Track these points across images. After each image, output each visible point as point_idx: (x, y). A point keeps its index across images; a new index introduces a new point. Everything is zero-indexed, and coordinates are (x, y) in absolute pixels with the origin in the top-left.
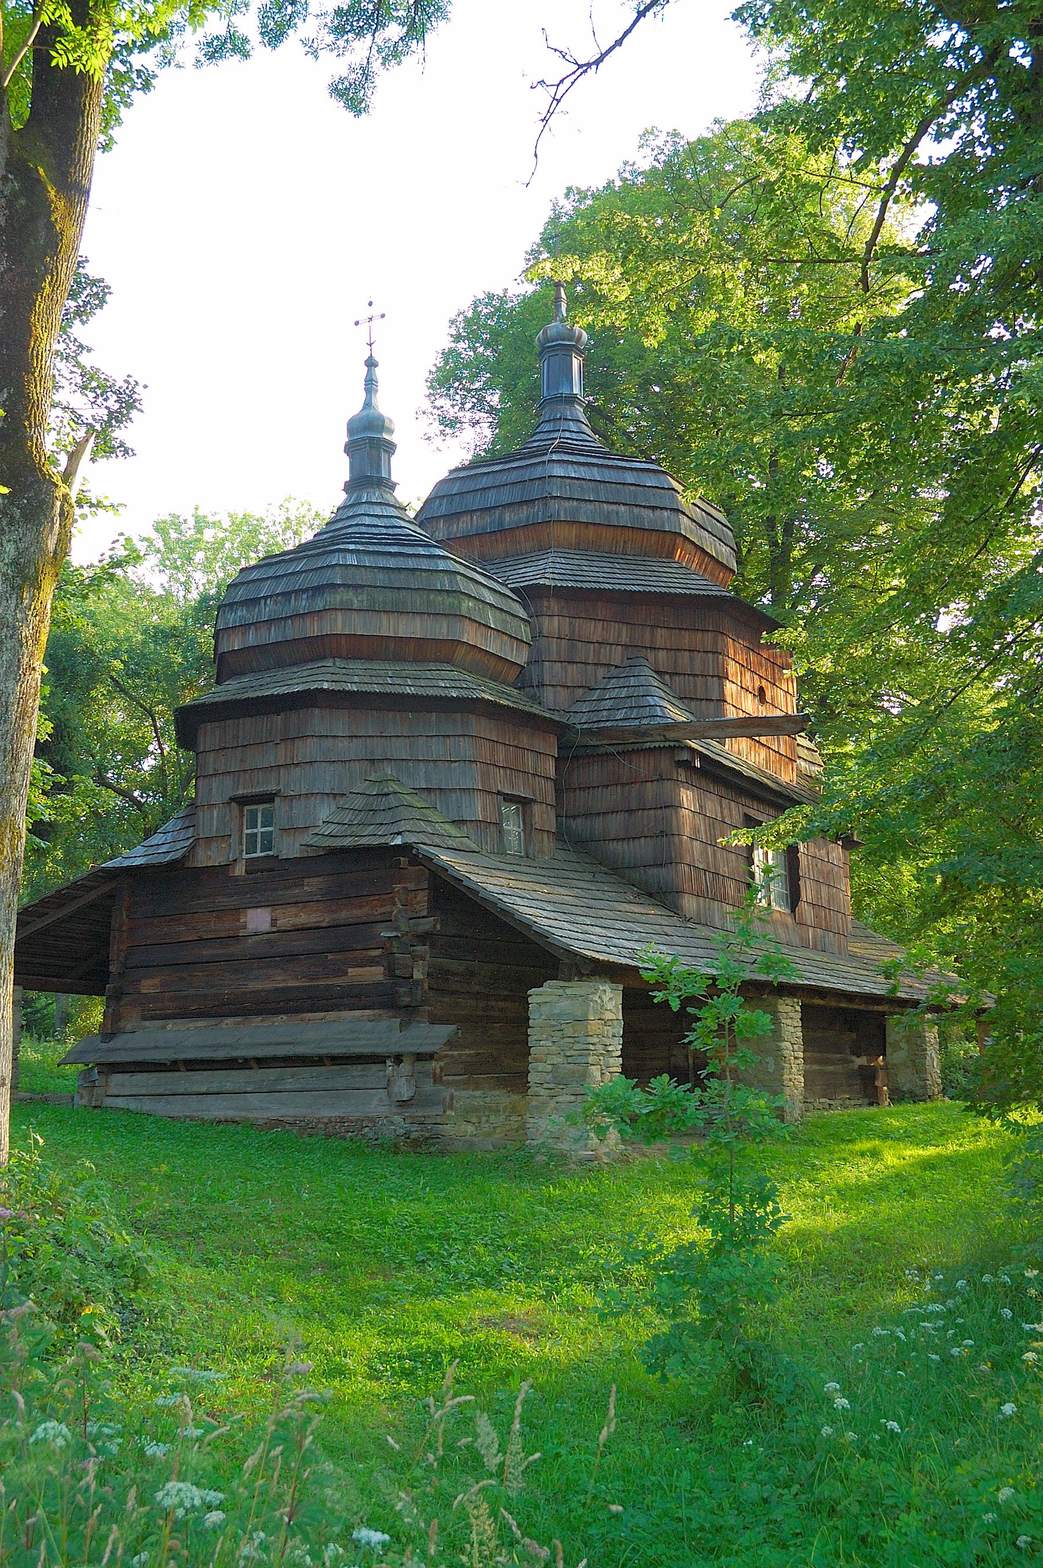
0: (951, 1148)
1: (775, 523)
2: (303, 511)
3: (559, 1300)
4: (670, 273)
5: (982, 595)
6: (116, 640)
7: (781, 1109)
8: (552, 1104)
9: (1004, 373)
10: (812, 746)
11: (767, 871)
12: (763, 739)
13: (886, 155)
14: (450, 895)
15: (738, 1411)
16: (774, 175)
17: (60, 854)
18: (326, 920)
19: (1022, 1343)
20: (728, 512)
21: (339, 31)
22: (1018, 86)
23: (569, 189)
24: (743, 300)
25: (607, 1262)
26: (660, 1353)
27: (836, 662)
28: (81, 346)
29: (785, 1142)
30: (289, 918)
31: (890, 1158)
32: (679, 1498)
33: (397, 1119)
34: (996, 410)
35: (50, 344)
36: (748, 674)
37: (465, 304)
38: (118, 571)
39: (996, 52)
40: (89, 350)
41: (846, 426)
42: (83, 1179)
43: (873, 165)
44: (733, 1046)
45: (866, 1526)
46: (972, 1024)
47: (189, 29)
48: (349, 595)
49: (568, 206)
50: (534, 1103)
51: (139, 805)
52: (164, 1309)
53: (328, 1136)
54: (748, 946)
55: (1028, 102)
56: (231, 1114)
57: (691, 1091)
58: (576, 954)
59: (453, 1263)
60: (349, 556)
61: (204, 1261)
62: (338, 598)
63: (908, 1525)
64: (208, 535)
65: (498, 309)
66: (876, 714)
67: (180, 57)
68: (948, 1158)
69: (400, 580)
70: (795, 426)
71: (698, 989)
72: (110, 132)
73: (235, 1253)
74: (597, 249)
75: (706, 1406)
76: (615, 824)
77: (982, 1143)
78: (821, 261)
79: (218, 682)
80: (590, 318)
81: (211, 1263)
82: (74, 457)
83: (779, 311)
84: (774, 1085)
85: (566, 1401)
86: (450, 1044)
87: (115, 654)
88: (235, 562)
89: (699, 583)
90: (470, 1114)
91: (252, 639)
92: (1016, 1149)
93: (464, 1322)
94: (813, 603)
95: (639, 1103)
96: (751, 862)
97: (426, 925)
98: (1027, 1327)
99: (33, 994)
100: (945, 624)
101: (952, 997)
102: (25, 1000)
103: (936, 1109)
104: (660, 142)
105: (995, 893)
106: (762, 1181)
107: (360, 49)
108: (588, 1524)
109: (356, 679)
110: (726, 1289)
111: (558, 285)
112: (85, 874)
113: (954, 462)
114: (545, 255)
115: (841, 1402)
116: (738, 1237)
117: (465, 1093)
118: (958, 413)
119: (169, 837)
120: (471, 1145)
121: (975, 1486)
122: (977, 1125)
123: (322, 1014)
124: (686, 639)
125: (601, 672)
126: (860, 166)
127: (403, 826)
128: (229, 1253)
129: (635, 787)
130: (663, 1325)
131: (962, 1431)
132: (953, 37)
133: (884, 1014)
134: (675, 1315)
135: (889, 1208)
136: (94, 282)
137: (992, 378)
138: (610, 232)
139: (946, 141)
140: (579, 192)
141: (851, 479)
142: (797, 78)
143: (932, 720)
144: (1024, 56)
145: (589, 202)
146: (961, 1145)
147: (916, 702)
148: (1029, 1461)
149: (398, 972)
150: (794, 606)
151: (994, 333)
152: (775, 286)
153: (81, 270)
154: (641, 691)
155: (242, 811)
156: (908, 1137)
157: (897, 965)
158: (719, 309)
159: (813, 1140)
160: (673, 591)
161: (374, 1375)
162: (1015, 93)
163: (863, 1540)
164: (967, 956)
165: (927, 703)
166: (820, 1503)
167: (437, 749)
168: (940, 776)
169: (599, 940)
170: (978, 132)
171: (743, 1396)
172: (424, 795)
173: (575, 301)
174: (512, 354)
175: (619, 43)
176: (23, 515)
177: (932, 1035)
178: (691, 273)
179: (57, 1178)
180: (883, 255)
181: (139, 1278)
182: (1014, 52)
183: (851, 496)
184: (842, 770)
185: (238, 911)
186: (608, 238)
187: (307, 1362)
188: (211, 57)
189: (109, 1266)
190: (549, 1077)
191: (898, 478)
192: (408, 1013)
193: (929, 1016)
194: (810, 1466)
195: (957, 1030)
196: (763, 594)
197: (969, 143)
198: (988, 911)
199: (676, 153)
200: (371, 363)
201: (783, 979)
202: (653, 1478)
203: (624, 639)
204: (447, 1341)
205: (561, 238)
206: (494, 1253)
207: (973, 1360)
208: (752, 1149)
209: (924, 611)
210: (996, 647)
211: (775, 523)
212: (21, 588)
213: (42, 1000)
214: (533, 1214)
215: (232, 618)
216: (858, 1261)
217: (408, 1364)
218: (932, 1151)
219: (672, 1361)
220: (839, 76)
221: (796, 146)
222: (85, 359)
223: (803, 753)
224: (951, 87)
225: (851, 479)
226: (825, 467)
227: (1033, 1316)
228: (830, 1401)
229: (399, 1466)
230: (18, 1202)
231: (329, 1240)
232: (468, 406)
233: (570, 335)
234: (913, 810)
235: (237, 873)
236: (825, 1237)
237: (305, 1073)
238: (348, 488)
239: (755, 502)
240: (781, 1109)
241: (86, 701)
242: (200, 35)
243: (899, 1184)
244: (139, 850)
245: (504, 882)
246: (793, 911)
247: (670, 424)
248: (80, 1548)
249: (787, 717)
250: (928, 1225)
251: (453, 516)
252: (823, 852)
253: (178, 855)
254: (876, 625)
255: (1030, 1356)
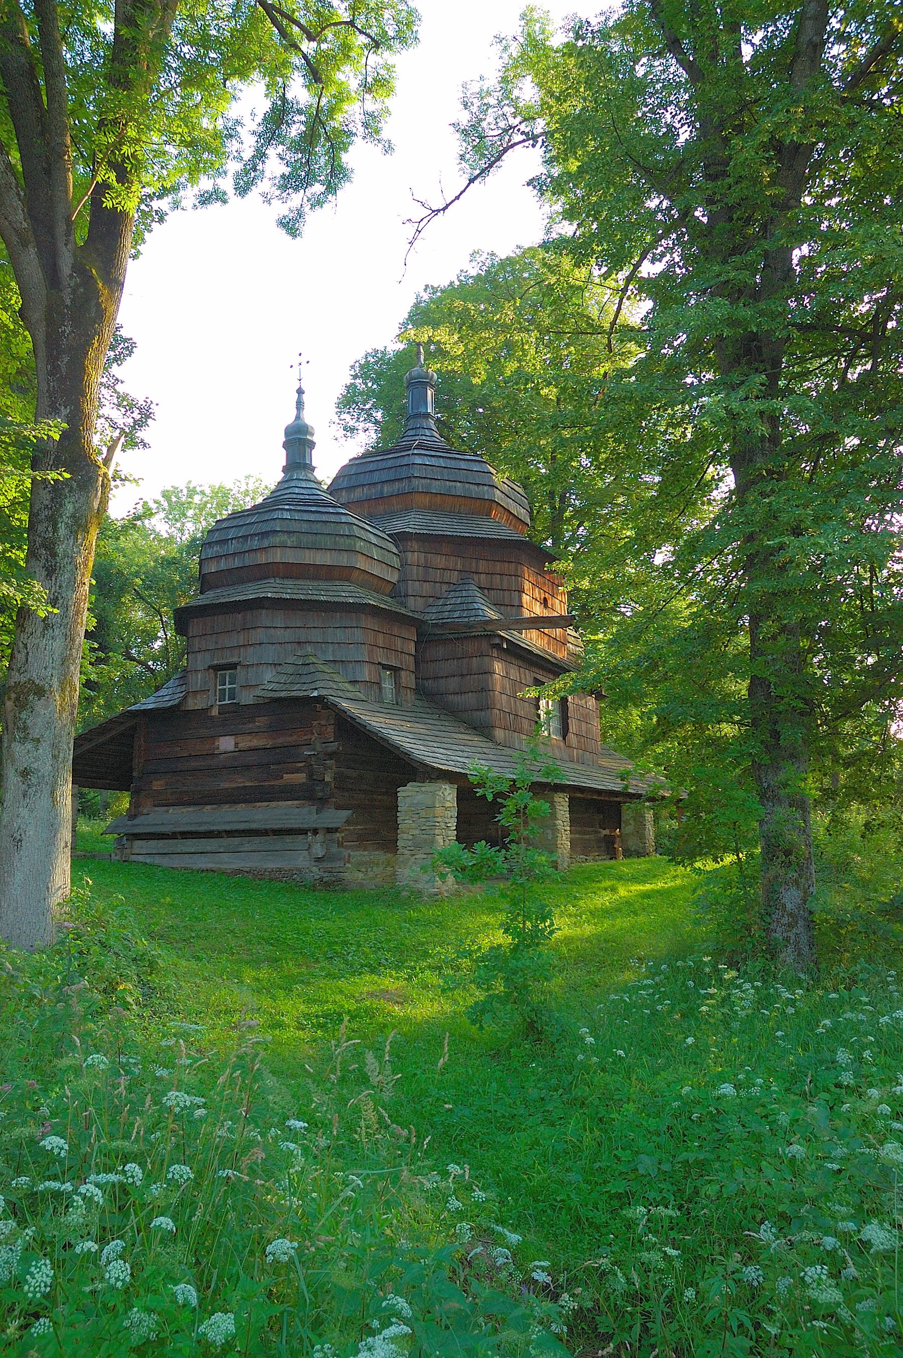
0: (660, 885)
1: (556, 489)
2: (257, 484)
3: (416, 981)
4: (489, 338)
5: (681, 542)
6: (137, 566)
7: (556, 862)
8: (413, 859)
9: (695, 405)
10: (576, 635)
11: (548, 713)
12: (546, 631)
13: (622, 270)
14: (349, 728)
15: (526, 1046)
16: (553, 280)
17: (102, 702)
18: (270, 743)
19: (699, 1001)
20: (525, 488)
21: (283, 187)
22: (699, 233)
23: (427, 286)
24: (534, 357)
25: (446, 957)
26: (478, 1013)
27: (591, 582)
28: (117, 379)
29: (558, 883)
30: (246, 743)
31: (622, 892)
32: (490, 1099)
33: (315, 869)
34: (690, 427)
35: (97, 378)
36: (537, 589)
37: (359, 356)
38: (139, 523)
39: (686, 213)
40: (122, 382)
41: (597, 435)
42: (118, 906)
43: (614, 276)
44: (526, 823)
45: (602, 1112)
46: (674, 808)
47: (189, 185)
48: (284, 537)
49: (426, 296)
50: (401, 859)
51: (152, 671)
52: (169, 986)
53: (271, 880)
54: (536, 760)
55: (706, 243)
56: (210, 866)
57: (499, 851)
58: (427, 765)
59: (350, 958)
60: (285, 513)
61: (194, 957)
62: (278, 540)
63: (628, 1110)
64: (197, 499)
65: (381, 359)
66: (617, 616)
67: (184, 203)
68: (658, 891)
69: (317, 528)
70: (566, 434)
71: (505, 788)
72: (138, 247)
73: (213, 952)
74: (443, 323)
75: (508, 1044)
76: (453, 684)
77: (678, 882)
78: (582, 333)
79: (202, 593)
80: (439, 365)
81: (198, 959)
82: (111, 450)
83: (556, 362)
84: (551, 847)
85: (421, 1041)
86: (348, 822)
87: (137, 574)
88: (214, 516)
89: (507, 532)
90: (361, 866)
91: (223, 565)
92: (699, 885)
93: (357, 995)
94: (578, 546)
95: (466, 859)
96: (538, 708)
97: (333, 747)
98: (703, 992)
99: (86, 790)
100: (659, 560)
101: (661, 792)
102: (81, 794)
103: (648, 862)
104: (483, 259)
105: (689, 727)
106: (543, 907)
107: (296, 199)
108: (433, 1115)
109: (289, 591)
110: (520, 973)
111: (419, 344)
112: (117, 715)
113: (665, 459)
114: (410, 326)
115: (590, 1040)
116: (526, 941)
117: (358, 853)
118: (667, 429)
119: (170, 691)
120: (361, 886)
121: (669, 1086)
122: (675, 871)
123: (267, 804)
124: (498, 567)
125: (445, 587)
126: (606, 276)
127: (318, 684)
128: (209, 952)
129: (465, 661)
130: (480, 995)
131: (662, 1054)
132: (661, 202)
133: (619, 803)
134: (488, 989)
135: (622, 922)
136: (126, 340)
137: (687, 408)
138: (451, 312)
139: (657, 263)
140: (433, 287)
141: (601, 468)
142: (568, 223)
143: (651, 619)
144: (703, 216)
145: (439, 294)
146: (666, 883)
147: (641, 608)
148: (701, 1071)
149: (315, 777)
150: (566, 547)
151: (689, 380)
152: (554, 348)
153: (118, 333)
154: (470, 600)
155: (216, 675)
156: (635, 879)
157: (628, 773)
158: (519, 361)
159: (574, 883)
160: (490, 537)
161: (301, 1027)
162: (698, 237)
163: (601, 1120)
164: (672, 766)
165: (648, 608)
166: (576, 1099)
167: (340, 635)
168: (655, 655)
169: (442, 757)
170: (677, 259)
171: (530, 1037)
172: (332, 665)
173: (428, 354)
174: (390, 386)
175: (457, 198)
176: (78, 486)
177: (649, 816)
178: (502, 338)
179: (100, 905)
180: (620, 331)
181: (152, 966)
182: (697, 214)
183: (601, 479)
184: (596, 650)
185: (214, 737)
186: (449, 315)
187: (260, 1020)
188: (203, 203)
189: (134, 960)
190: (410, 843)
191: (630, 468)
192: (321, 802)
193: (647, 804)
194: (570, 1078)
195: (665, 813)
196: (546, 539)
197: (672, 265)
198: (685, 739)
199: (493, 265)
200: (300, 392)
201: (557, 781)
202: (474, 1087)
203: (459, 567)
204: (346, 1006)
205: (420, 316)
206: (375, 952)
207: (670, 1013)
208: (536, 887)
209: (646, 551)
210: (690, 574)
211: (556, 489)
212: (76, 532)
213: (91, 793)
214: (401, 928)
215: (210, 552)
216: (602, 955)
217: (322, 1020)
218: (648, 887)
219: (487, 1017)
220: (593, 222)
221: (566, 262)
222: (119, 387)
223: (571, 639)
224: (660, 232)
225: (601, 468)
226: (585, 461)
227: (706, 985)
228: (583, 1039)
229: (319, 1079)
230: (76, 920)
231: (272, 945)
232: (362, 419)
233: (426, 375)
234: (638, 676)
235: (213, 714)
236: (582, 940)
237: (256, 840)
238: (285, 470)
239: (541, 481)
240: (556, 862)
241: (118, 605)
242: (196, 190)
243: (627, 907)
244: (152, 699)
245: (383, 720)
246: (564, 739)
247: (489, 433)
248: (118, 1130)
249: (561, 616)
250: (645, 932)
251: (350, 489)
252: (583, 702)
253: (176, 702)
254: (617, 560)
255: (704, 1008)
